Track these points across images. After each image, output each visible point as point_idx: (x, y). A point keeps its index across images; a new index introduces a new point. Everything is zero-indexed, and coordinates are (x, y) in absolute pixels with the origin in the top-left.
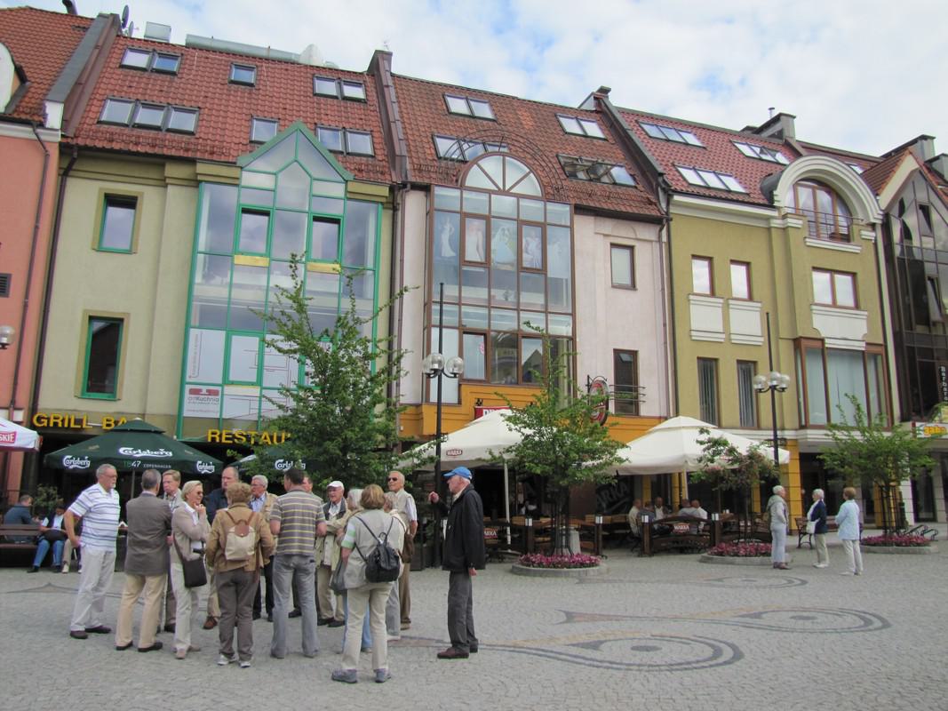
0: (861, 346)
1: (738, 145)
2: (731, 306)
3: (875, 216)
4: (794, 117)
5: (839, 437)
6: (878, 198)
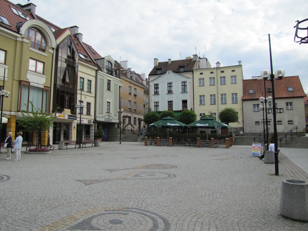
0: (42, 87)
1: (12, 8)
2: (28, 73)
3: (54, 46)
4: (36, 6)
5: (25, 115)
6: (56, 40)
